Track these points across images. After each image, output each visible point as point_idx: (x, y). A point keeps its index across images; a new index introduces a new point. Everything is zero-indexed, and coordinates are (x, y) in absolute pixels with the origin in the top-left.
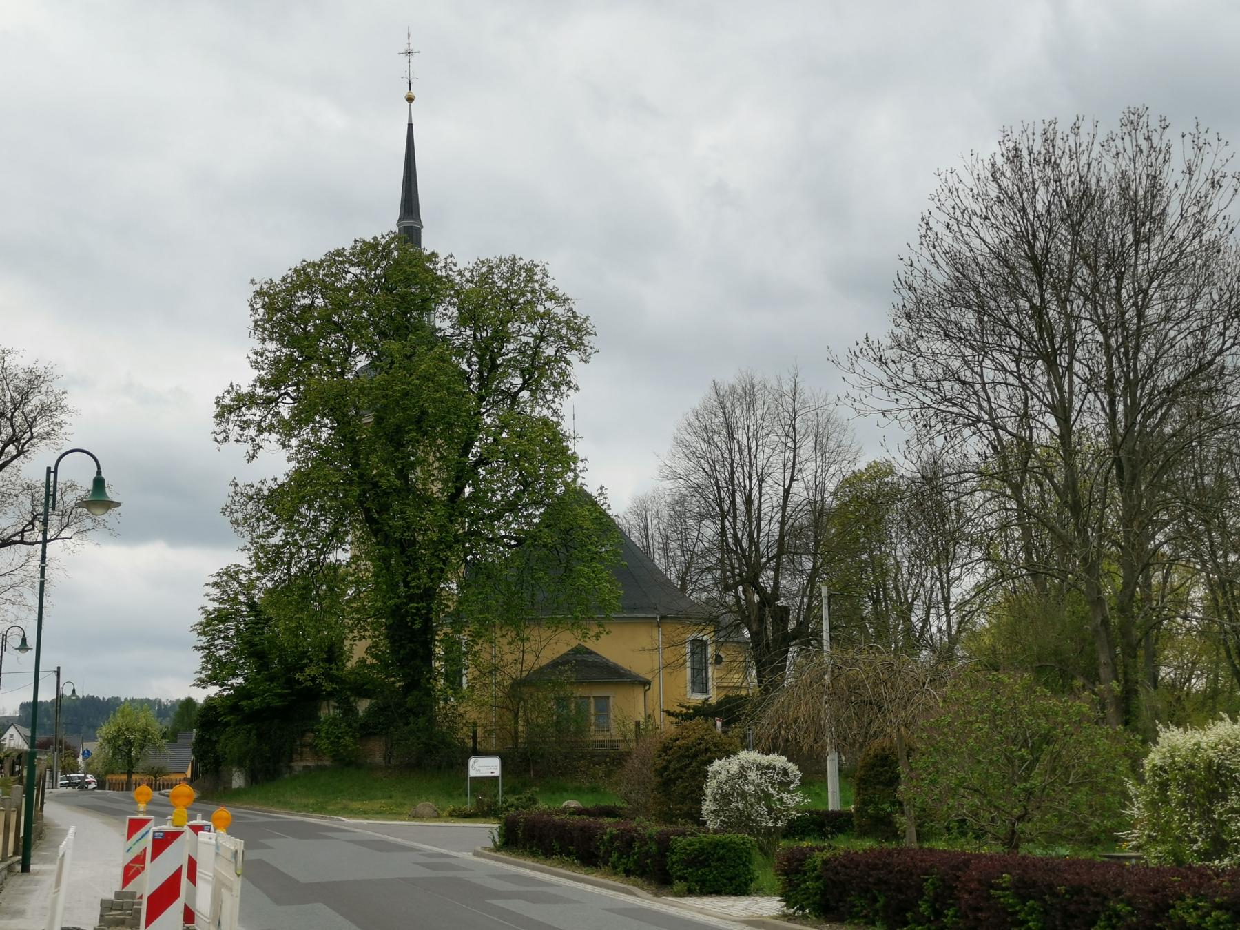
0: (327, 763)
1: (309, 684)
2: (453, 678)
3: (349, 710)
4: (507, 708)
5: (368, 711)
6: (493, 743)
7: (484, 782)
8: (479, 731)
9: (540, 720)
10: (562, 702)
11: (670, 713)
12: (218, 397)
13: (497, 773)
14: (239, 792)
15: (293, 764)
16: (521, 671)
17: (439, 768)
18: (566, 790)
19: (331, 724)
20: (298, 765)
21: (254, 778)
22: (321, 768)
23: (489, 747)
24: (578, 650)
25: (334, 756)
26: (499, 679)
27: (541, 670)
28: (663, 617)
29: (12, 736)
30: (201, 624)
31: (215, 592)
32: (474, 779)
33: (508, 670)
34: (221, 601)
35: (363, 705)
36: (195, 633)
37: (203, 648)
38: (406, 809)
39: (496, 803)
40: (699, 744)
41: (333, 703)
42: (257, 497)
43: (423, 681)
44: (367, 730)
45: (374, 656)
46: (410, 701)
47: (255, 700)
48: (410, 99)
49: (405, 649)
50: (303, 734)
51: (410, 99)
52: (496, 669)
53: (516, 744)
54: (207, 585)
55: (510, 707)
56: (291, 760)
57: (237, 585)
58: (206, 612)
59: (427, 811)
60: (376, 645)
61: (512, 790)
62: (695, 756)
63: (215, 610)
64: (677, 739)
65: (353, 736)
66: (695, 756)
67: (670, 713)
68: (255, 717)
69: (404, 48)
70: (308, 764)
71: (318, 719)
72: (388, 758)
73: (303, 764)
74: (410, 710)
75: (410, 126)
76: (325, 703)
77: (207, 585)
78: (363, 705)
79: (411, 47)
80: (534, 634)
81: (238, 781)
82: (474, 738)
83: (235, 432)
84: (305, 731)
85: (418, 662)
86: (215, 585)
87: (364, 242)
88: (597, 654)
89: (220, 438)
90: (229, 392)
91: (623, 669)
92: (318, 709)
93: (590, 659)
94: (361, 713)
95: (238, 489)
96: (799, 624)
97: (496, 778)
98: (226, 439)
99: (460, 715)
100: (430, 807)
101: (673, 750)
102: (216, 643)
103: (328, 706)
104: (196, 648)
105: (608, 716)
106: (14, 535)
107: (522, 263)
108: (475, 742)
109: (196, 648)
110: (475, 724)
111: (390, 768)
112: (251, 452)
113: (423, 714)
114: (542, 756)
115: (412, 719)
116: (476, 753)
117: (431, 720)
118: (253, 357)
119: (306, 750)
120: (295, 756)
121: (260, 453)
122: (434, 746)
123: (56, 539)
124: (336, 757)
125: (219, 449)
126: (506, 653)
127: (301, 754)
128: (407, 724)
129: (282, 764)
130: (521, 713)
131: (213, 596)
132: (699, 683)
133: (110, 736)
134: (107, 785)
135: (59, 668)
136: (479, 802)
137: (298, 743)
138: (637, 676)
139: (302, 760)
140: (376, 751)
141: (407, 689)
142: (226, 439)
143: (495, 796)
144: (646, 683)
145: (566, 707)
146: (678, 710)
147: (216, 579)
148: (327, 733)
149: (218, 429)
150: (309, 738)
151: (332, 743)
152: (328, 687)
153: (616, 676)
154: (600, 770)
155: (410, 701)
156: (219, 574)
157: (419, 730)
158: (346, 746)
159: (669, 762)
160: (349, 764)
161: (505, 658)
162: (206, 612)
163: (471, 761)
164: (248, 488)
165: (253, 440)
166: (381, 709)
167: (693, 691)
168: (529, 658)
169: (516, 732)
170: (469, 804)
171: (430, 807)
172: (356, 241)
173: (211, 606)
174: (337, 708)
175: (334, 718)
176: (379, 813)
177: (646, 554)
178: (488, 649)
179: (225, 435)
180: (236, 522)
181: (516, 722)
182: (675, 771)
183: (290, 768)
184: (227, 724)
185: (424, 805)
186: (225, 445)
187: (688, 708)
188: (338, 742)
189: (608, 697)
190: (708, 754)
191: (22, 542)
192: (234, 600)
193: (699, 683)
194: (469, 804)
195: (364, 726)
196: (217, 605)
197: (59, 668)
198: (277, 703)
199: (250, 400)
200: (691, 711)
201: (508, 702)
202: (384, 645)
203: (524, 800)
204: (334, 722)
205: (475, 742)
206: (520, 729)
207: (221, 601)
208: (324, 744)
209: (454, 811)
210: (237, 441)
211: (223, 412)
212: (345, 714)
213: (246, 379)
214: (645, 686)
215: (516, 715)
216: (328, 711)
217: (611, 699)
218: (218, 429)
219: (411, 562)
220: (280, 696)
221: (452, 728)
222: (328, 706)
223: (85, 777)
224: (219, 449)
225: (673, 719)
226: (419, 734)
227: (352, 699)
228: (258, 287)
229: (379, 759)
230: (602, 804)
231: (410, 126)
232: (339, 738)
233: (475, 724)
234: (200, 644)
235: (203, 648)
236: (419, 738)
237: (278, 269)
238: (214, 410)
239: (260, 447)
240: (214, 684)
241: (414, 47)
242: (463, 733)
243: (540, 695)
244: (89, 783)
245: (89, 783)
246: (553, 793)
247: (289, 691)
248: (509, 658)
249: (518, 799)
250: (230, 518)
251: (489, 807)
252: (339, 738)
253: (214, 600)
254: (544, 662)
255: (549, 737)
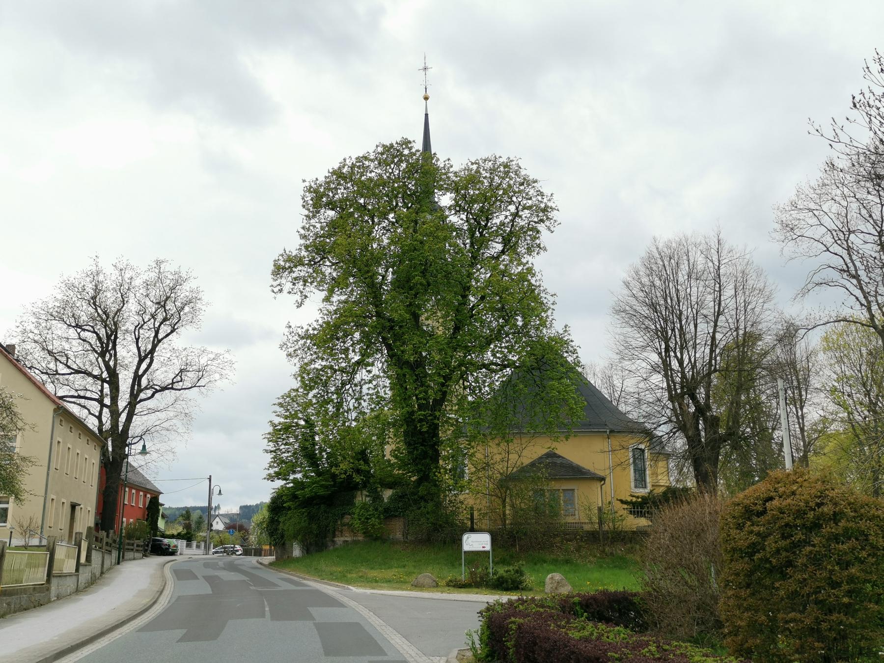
0: (360, 538)
1: (343, 476)
2: (456, 472)
3: (377, 497)
4: (497, 496)
5: (390, 498)
6: (486, 524)
7: (476, 556)
8: (476, 514)
9: (523, 505)
10: (540, 493)
11: (622, 502)
12: (275, 261)
13: (488, 547)
14: (297, 560)
15: (336, 539)
16: (507, 468)
17: (445, 543)
18: (545, 562)
19: (362, 508)
20: (339, 540)
21: (307, 550)
22: (355, 542)
23: (483, 527)
24: (551, 455)
25: (364, 533)
26: (490, 473)
27: (523, 470)
28: (612, 431)
29: (217, 522)
30: (269, 434)
31: (281, 410)
32: (465, 552)
33: (496, 466)
34: (286, 417)
35: (387, 494)
36: (266, 440)
37: (271, 452)
38: (412, 579)
39: (487, 574)
40: (819, 505)
41: (365, 492)
42: (307, 336)
43: (431, 474)
44: (389, 514)
45: (396, 457)
46: (422, 491)
47: (306, 490)
48: (426, 98)
49: (417, 450)
50: (342, 517)
51: (426, 98)
52: (488, 464)
53: (505, 525)
54: (274, 404)
55: (499, 495)
56: (334, 536)
57: (296, 405)
58: (274, 425)
59: (428, 581)
60: (398, 449)
61: (503, 562)
62: (815, 526)
63: (280, 423)
64: (771, 499)
65: (379, 518)
66: (815, 526)
67: (622, 502)
68: (309, 502)
69: (422, 66)
70: (346, 539)
71: (353, 504)
72: (406, 535)
73: (342, 539)
74: (422, 498)
75: (427, 115)
76: (359, 493)
77: (274, 404)
78: (387, 494)
79: (426, 65)
80: (515, 446)
81: (297, 552)
82: (472, 519)
83: (288, 286)
84: (344, 514)
85: (428, 461)
86: (280, 405)
87: (383, 145)
88: (564, 458)
89: (276, 290)
90: (282, 255)
91: (584, 468)
92: (354, 497)
93: (559, 461)
94: (386, 501)
95: (291, 330)
96: (729, 428)
97: (487, 552)
98: (281, 291)
99: (462, 503)
100: (430, 577)
101: (768, 517)
102: (281, 448)
103: (362, 495)
104: (266, 451)
105: (573, 504)
106: (169, 385)
107: (501, 160)
108: (472, 523)
109: (266, 451)
110: (472, 508)
111: (406, 542)
112: (300, 301)
113: (432, 500)
114: (525, 534)
115: (422, 504)
116: (472, 530)
117: (438, 505)
118: (302, 232)
119: (345, 528)
120: (337, 533)
121: (307, 301)
122: (440, 525)
123: (195, 386)
124: (366, 533)
125: (275, 298)
126: (495, 454)
127: (341, 532)
128: (419, 508)
129: (328, 539)
130: (508, 500)
131: (278, 413)
132: (641, 480)
133: (259, 522)
134: (263, 552)
135: (210, 476)
136: (471, 573)
137: (339, 523)
138: (594, 474)
139: (342, 536)
140: (397, 529)
141: (419, 482)
142: (281, 291)
143: (487, 569)
144: (602, 479)
145: (543, 495)
146: (629, 499)
147: (281, 401)
148: (358, 515)
149: (275, 283)
150: (347, 519)
151: (362, 523)
152: (358, 479)
153: (578, 474)
154: (572, 545)
155: (422, 491)
156: (283, 397)
157: (428, 513)
158: (373, 525)
159: (764, 536)
160: (376, 539)
161: (495, 457)
162: (274, 425)
163: (465, 537)
164: (299, 329)
165: (301, 292)
166: (400, 497)
167: (636, 487)
168: (513, 457)
169: (504, 514)
170: (463, 575)
171: (430, 577)
172: (377, 146)
173: (277, 420)
174: (368, 496)
175: (365, 504)
176: (389, 582)
177: (595, 387)
178: (481, 450)
179: (279, 287)
180: (289, 355)
181: (504, 507)
182: (778, 551)
183: (333, 542)
184: (289, 508)
185: (426, 575)
186: (279, 295)
187: (638, 497)
188: (367, 522)
189: (573, 490)
190: (843, 523)
191: (172, 388)
192: (294, 416)
193: (641, 480)
194: (463, 575)
195: (387, 510)
196: (282, 420)
197: (210, 476)
198: (322, 492)
199: (298, 261)
200: (640, 500)
201: (497, 491)
202: (402, 446)
203: (513, 572)
204: (364, 506)
205: (472, 523)
206: (507, 512)
207: (286, 417)
208: (357, 524)
209: (451, 581)
210: (290, 293)
211: (278, 270)
212: (374, 500)
213: (294, 245)
214: (601, 481)
215: (504, 501)
216: (362, 498)
217: (576, 491)
218: (275, 283)
219: (420, 380)
220: (326, 487)
221: (455, 511)
222: (362, 495)
223: (234, 547)
224: (275, 298)
225: (625, 506)
226: (428, 516)
227: (379, 489)
228: (307, 184)
229: (399, 536)
230: (612, 589)
231: (427, 115)
232: (368, 519)
233: (472, 508)
234: (270, 448)
235: (271, 452)
236: (428, 519)
237: (320, 173)
238: (272, 268)
239: (306, 297)
240: (279, 479)
241: (428, 65)
242: (464, 516)
243: (522, 486)
244: (237, 551)
245: (237, 551)
246: (535, 564)
247: (332, 483)
248: (498, 458)
249: (507, 571)
250: (286, 352)
251: (481, 578)
252: (368, 519)
253: (278, 416)
254: (526, 461)
255: (530, 519)
